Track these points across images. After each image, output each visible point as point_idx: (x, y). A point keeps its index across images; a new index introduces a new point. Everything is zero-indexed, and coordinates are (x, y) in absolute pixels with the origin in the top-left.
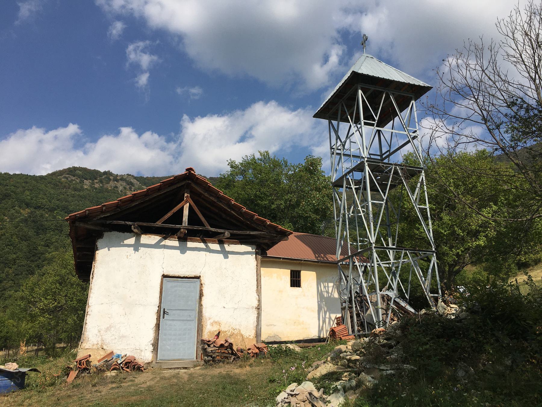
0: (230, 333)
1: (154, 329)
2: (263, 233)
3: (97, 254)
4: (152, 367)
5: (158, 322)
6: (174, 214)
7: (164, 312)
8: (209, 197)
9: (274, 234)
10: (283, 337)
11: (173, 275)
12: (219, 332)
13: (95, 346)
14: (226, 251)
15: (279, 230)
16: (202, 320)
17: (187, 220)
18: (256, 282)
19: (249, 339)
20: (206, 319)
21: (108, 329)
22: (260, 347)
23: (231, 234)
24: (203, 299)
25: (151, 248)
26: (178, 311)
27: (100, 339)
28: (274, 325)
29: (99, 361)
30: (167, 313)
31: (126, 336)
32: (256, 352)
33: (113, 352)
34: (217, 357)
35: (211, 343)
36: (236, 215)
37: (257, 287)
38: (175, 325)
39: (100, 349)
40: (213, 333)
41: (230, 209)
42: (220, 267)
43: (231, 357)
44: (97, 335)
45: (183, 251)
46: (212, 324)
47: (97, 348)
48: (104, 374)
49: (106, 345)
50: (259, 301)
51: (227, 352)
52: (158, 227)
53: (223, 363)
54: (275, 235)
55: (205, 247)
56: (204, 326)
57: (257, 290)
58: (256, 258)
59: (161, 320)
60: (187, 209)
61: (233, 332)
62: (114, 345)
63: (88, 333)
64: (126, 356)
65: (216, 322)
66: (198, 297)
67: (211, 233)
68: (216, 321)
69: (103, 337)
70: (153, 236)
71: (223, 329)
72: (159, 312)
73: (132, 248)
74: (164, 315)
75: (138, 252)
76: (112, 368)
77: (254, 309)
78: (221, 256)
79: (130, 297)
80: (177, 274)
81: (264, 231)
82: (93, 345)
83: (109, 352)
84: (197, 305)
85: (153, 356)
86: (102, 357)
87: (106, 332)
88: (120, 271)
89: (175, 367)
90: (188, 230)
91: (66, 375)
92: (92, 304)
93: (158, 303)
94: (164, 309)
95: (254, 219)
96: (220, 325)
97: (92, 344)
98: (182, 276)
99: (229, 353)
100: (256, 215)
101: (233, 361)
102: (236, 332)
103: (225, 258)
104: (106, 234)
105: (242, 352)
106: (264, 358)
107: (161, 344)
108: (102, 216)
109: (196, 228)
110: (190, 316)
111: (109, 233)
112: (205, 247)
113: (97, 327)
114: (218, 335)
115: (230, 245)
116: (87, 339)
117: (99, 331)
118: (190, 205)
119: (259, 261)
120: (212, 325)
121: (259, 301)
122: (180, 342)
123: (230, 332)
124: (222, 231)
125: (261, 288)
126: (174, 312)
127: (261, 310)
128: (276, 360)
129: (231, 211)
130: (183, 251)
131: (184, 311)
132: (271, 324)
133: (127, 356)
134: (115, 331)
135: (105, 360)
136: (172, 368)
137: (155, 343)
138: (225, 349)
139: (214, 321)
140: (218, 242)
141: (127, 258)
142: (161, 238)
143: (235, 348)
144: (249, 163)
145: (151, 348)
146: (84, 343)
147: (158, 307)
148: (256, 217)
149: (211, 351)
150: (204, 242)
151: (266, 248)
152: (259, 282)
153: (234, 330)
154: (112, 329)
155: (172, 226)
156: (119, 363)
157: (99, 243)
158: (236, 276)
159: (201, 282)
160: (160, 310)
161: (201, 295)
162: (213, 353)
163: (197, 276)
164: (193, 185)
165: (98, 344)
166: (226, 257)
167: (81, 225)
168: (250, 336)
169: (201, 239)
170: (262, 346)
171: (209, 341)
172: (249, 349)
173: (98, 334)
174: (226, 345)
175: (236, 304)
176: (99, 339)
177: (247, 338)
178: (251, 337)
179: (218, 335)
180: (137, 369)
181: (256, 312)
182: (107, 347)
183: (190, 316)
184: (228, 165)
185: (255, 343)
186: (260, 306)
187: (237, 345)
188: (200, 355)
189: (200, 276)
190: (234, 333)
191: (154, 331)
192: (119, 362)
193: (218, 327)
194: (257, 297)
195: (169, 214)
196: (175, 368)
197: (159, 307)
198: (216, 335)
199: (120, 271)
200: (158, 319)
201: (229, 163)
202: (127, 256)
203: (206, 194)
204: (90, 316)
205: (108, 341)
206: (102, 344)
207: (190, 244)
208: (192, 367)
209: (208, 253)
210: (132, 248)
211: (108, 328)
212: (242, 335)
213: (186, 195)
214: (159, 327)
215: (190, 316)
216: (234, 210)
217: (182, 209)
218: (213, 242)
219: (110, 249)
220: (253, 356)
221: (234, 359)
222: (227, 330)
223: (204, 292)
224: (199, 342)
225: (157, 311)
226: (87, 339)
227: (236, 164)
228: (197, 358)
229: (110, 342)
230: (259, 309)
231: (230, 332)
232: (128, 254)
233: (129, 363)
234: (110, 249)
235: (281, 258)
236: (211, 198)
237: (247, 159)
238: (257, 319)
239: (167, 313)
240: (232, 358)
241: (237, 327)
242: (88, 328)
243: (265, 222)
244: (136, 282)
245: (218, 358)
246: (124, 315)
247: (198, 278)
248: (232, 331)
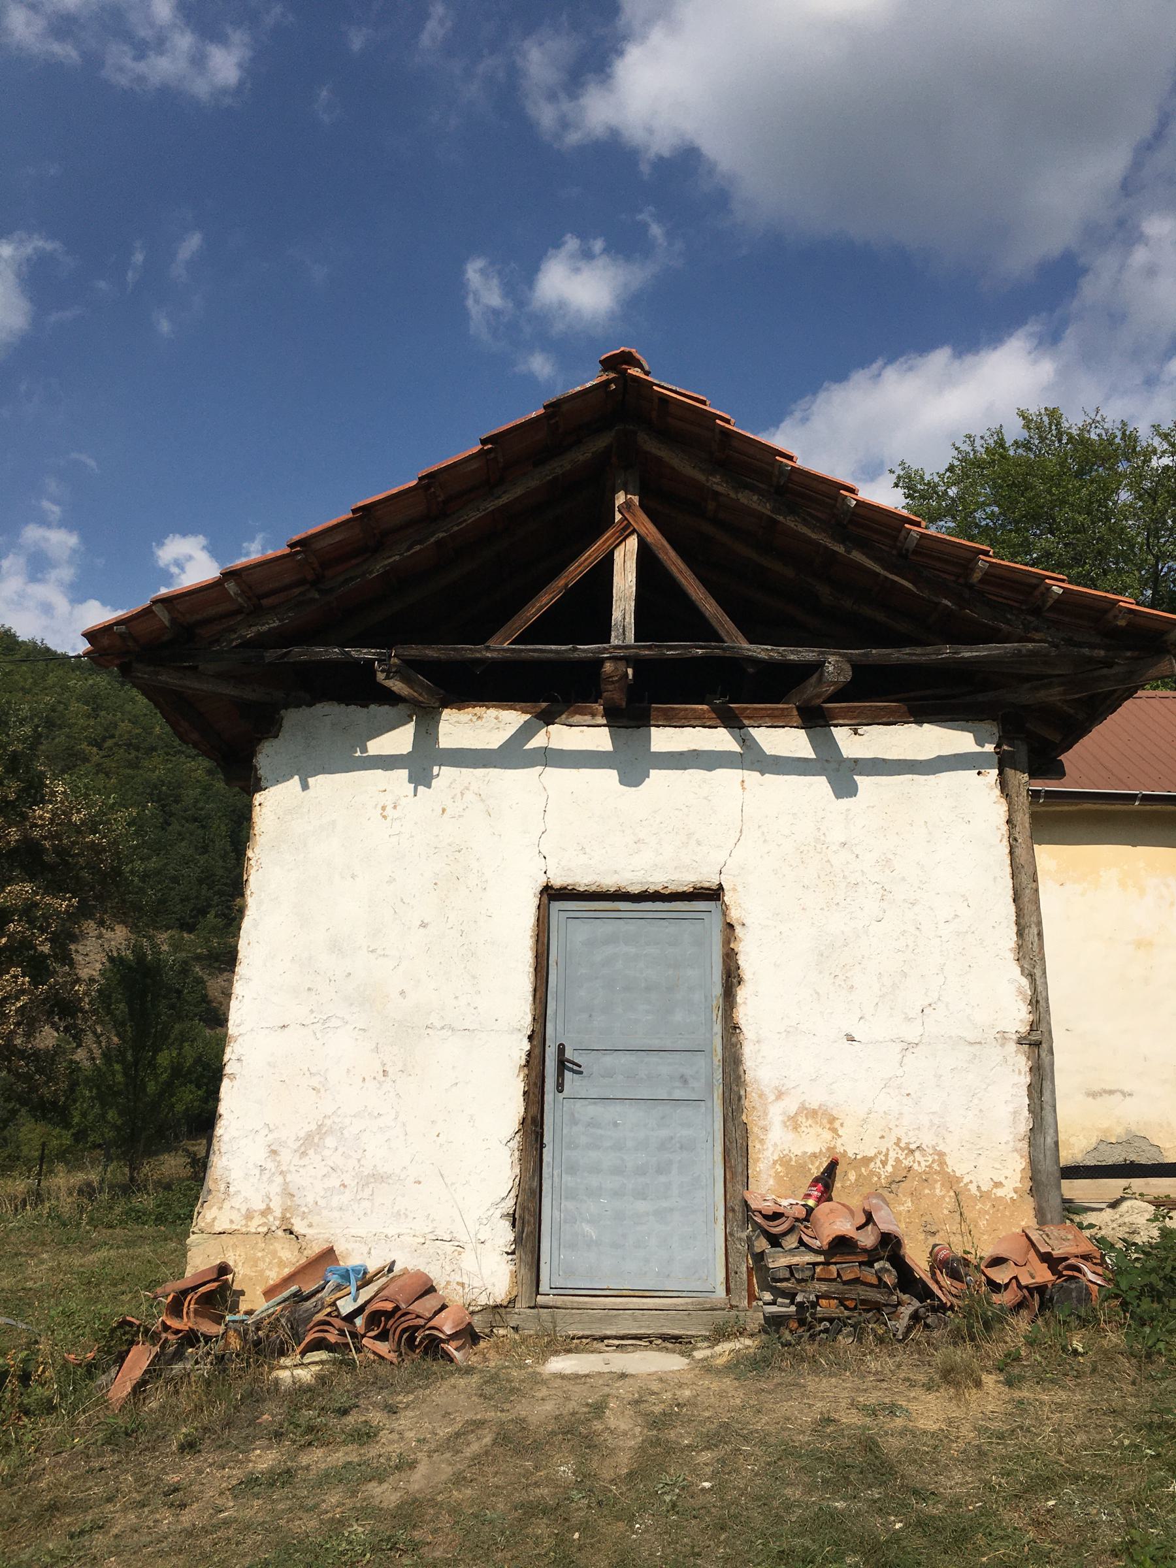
0: (889, 1168)
1: (514, 1144)
2: (1030, 646)
3: (258, 808)
4: (516, 1329)
5: (534, 1110)
6: (571, 593)
7: (562, 1064)
8: (733, 495)
9: (1092, 646)
10: (1168, 1146)
11: (593, 888)
12: (833, 1166)
13: (257, 1220)
14: (842, 761)
15: (1122, 623)
16: (745, 1102)
17: (630, 620)
18: (1012, 908)
19: (996, 1203)
20: (761, 1096)
21: (309, 1143)
22: (1056, 1253)
23: (856, 667)
24: (739, 999)
25: (485, 766)
26: (625, 1059)
27: (278, 1190)
28: (1124, 1094)
29: (269, 1293)
30: (575, 1068)
31: (389, 1177)
32: (1039, 1280)
33: (331, 1251)
34: (823, 1302)
35: (784, 1227)
36: (877, 569)
37: (1020, 933)
38: (616, 1125)
39: (280, 1233)
40: (802, 1167)
41: (842, 541)
42: (817, 840)
43: (900, 1303)
44: (262, 1169)
45: (632, 776)
46: (793, 1123)
47: (264, 1229)
48: (272, 1369)
49: (304, 1216)
50: (1038, 1003)
51: (874, 1281)
52: (494, 663)
53: (859, 1333)
54: (1102, 653)
55: (737, 748)
56: (754, 1130)
57: (1020, 947)
58: (1003, 784)
59: (548, 1098)
60: (632, 565)
61: (906, 1163)
62: (336, 1214)
63: (224, 1159)
64: (390, 1270)
65: (813, 1114)
66: (718, 990)
67: (751, 670)
68: (815, 1106)
69: (289, 1178)
70: (492, 712)
71: (850, 1145)
72: (534, 1064)
73: (404, 773)
74: (560, 1074)
75: (429, 787)
76: (307, 1340)
77: (1012, 1047)
78: (820, 785)
79: (402, 993)
80: (609, 882)
81: (1037, 636)
82: (249, 1216)
83: (316, 1249)
84: (718, 1028)
85: (515, 1274)
86: (287, 1271)
87: (304, 1154)
88: (353, 877)
89: (622, 1332)
90: (638, 663)
91: (115, 1362)
92: (242, 1030)
93: (529, 1018)
94: (561, 1049)
95: (977, 576)
96: (837, 1124)
97: (243, 1211)
98: (635, 889)
99: (881, 1284)
100: (986, 553)
101: (909, 1329)
102: (920, 1163)
103: (838, 796)
104: (291, 717)
105: (955, 1275)
106: (1084, 1322)
107: (556, 1213)
108: (250, 634)
109: (672, 650)
110: (684, 1080)
111: (305, 711)
112: (736, 747)
113: (266, 1131)
114: (826, 1181)
115: (862, 730)
116: (222, 1187)
117: (274, 1152)
118: (642, 544)
119: (1023, 800)
120: (796, 1128)
121: (1038, 1003)
122: (642, 1206)
123: (891, 1162)
124: (808, 655)
125: (1040, 935)
126: (608, 1060)
127: (1051, 1052)
128: (1161, 1345)
129: (849, 552)
130: (632, 776)
131: (654, 1059)
132: (1108, 1088)
133: (397, 1269)
134: (341, 1150)
135: (286, 1294)
136: (608, 1338)
137: (523, 1209)
138: (861, 1264)
139: (803, 1108)
140: (797, 720)
141: (385, 817)
142: (528, 716)
143: (918, 1257)
144: (978, 464)
145: (505, 1234)
146: (211, 1208)
147: (530, 1038)
148: (982, 562)
149: (789, 1267)
150: (732, 722)
151: (1056, 738)
152: (1028, 907)
153: (912, 1151)
154: (330, 1142)
155: (556, 652)
156: (344, 1312)
157: (266, 758)
158: (903, 879)
159: (724, 914)
160: (537, 1051)
161: (731, 978)
162: (799, 1281)
163: (707, 885)
164: (652, 446)
165: (269, 1208)
166: (844, 788)
167: (163, 678)
168: (998, 1185)
169: (714, 710)
170: (1074, 1250)
171: (776, 1216)
172: (997, 1261)
173: (270, 1165)
174: (867, 1239)
175: (909, 1019)
176: (275, 1188)
177: (984, 1196)
178: (1007, 1192)
179: (826, 1181)
180: (426, 1352)
181: (1022, 1063)
182: (310, 1226)
183: (685, 1082)
184: (896, 485)
185: (1026, 1219)
186: (1043, 1027)
187: (934, 1233)
188: (745, 1276)
189: (721, 887)
190: (910, 1169)
191: (517, 1154)
192: (346, 1306)
193: (827, 1135)
194: (1025, 982)
195: (545, 600)
196: (622, 1338)
197: (538, 1037)
198: (816, 1181)
199: (353, 877)
200: (534, 1096)
201: (899, 477)
202: (384, 808)
203: (717, 483)
204: (235, 1083)
205: (310, 1199)
206: (285, 1210)
207: (663, 739)
208: (706, 1338)
209: (752, 777)
210: (404, 773)
211: (309, 1136)
212: (951, 1182)
213: (620, 498)
214: (540, 1136)
215: (684, 1080)
216: (863, 545)
217: (606, 566)
218: (777, 721)
219: (311, 781)
220: (1020, 1306)
221: (915, 1317)
222: (871, 1154)
223: (747, 963)
224: (733, 1210)
225: (524, 1057)
226: (222, 1187)
227: (927, 478)
228: (728, 1291)
229: (321, 1203)
230: (1038, 1044)
231: (891, 1162)
232: (388, 799)
233: (389, 1315)
234: (311, 781)
235: (1133, 797)
236: (744, 500)
237: (969, 449)
238: (1030, 1096)
239: (575, 1068)
240: (906, 1311)
241: (927, 1139)
242: (225, 1138)
243: (1036, 586)
244: (424, 925)
245: (827, 1307)
246: (380, 1077)
247: (714, 894)
248: (897, 1160)
